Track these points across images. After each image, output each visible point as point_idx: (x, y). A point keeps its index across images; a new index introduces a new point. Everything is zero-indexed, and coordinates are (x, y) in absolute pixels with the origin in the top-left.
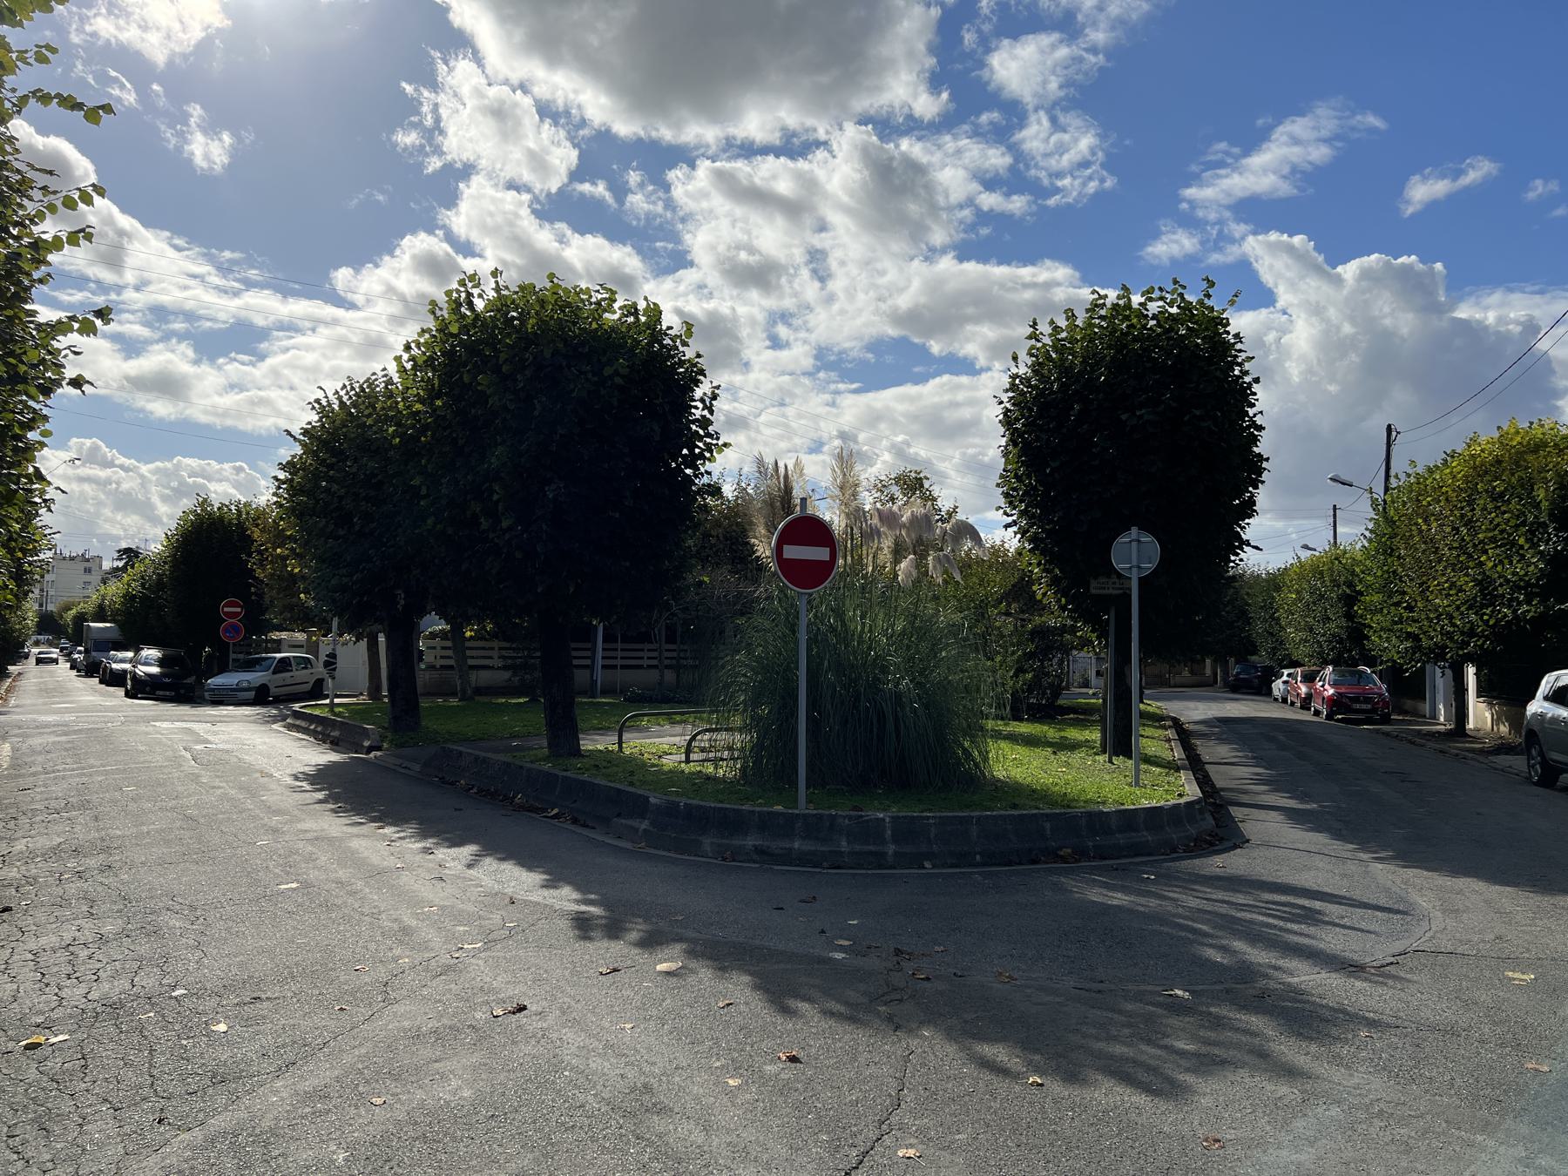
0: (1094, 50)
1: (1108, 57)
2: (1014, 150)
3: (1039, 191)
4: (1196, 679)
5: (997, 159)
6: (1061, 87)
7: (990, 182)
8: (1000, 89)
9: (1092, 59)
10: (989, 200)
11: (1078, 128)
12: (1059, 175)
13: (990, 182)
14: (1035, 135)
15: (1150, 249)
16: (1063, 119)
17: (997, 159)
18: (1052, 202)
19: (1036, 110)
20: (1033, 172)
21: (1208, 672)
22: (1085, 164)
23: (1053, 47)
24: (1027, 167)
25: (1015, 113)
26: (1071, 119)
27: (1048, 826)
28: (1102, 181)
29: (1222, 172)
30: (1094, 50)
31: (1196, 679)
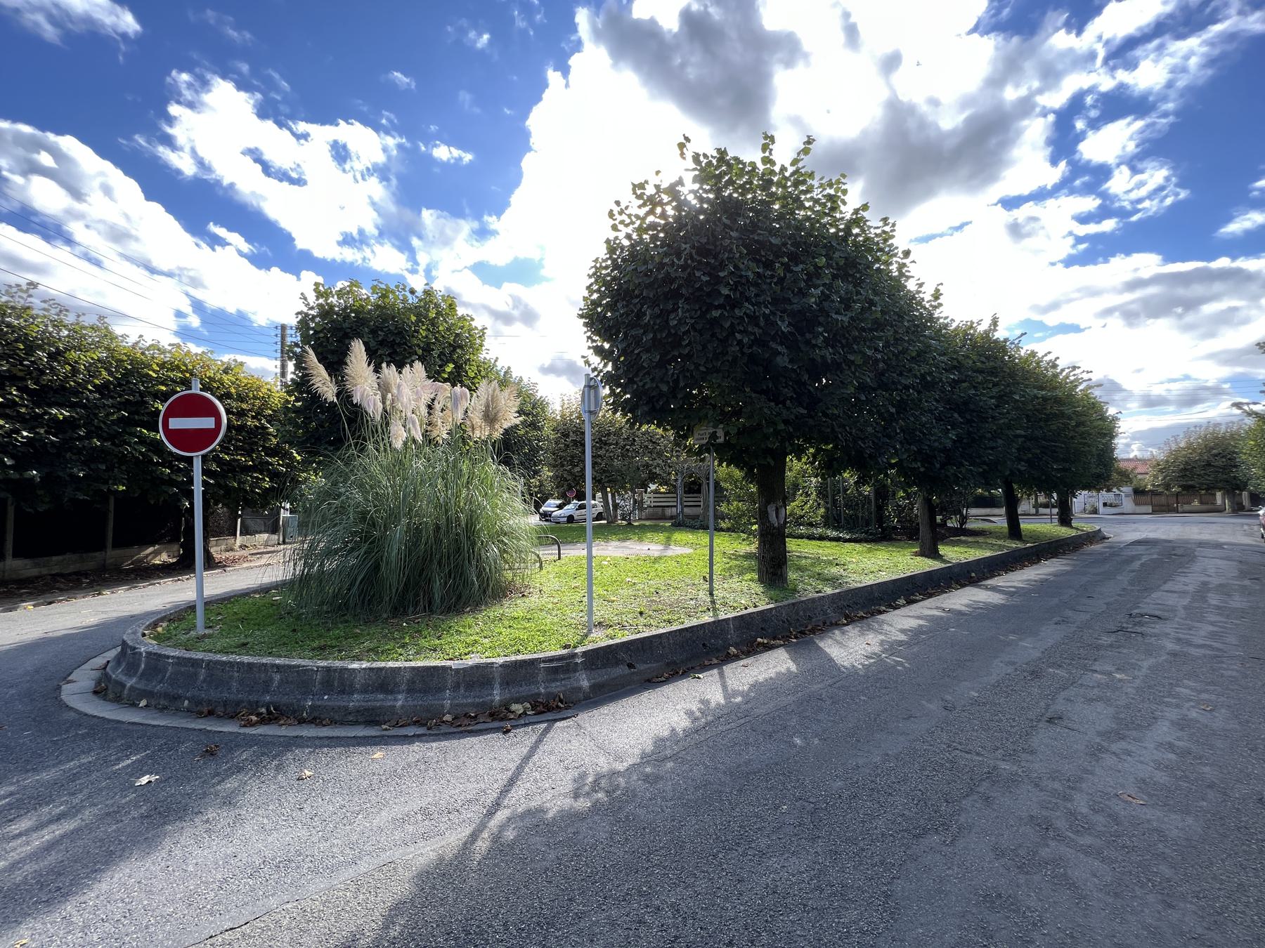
0: (1165, 115)
1: (68, 36)
2: (1104, 196)
3: (1122, 214)
4: (1205, 507)
5: (1090, 203)
6: (1137, 146)
7: (1083, 219)
8: (1089, 162)
9: (1164, 121)
10: (1092, 229)
11: (1153, 168)
12: (1140, 201)
13: (1083, 219)
14: (1120, 183)
15: (1223, 230)
16: (1140, 166)
17: (1090, 203)
18: (1135, 218)
19: (1118, 165)
20: (1117, 205)
21: (1219, 501)
22: (1161, 188)
23: (1129, 124)
24: (1113, 202)
25: (1102, 172)
26: (1149, 164)
27: (277, 677)
28: (1177, 194)
29: (993, 141)
30: (1165, 115)
31: (1205, 507)
